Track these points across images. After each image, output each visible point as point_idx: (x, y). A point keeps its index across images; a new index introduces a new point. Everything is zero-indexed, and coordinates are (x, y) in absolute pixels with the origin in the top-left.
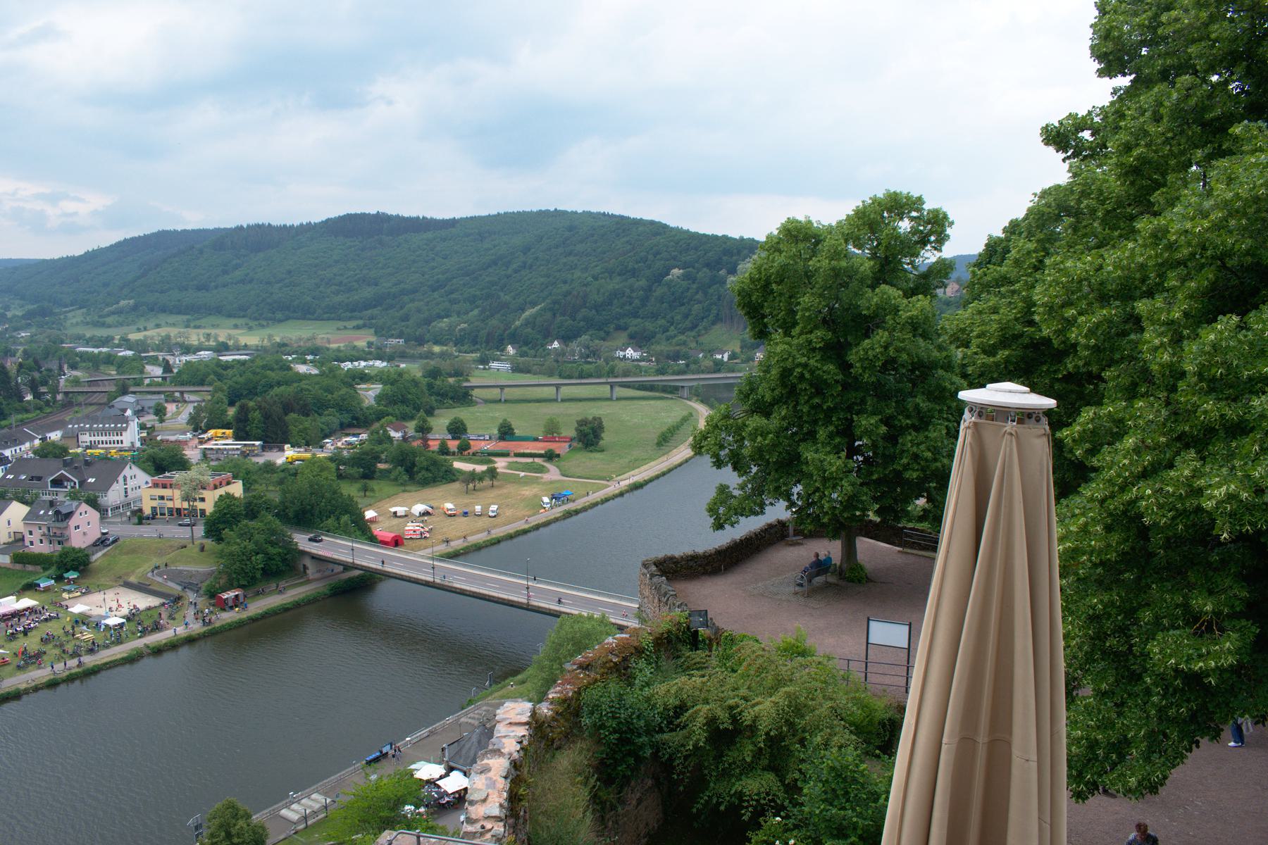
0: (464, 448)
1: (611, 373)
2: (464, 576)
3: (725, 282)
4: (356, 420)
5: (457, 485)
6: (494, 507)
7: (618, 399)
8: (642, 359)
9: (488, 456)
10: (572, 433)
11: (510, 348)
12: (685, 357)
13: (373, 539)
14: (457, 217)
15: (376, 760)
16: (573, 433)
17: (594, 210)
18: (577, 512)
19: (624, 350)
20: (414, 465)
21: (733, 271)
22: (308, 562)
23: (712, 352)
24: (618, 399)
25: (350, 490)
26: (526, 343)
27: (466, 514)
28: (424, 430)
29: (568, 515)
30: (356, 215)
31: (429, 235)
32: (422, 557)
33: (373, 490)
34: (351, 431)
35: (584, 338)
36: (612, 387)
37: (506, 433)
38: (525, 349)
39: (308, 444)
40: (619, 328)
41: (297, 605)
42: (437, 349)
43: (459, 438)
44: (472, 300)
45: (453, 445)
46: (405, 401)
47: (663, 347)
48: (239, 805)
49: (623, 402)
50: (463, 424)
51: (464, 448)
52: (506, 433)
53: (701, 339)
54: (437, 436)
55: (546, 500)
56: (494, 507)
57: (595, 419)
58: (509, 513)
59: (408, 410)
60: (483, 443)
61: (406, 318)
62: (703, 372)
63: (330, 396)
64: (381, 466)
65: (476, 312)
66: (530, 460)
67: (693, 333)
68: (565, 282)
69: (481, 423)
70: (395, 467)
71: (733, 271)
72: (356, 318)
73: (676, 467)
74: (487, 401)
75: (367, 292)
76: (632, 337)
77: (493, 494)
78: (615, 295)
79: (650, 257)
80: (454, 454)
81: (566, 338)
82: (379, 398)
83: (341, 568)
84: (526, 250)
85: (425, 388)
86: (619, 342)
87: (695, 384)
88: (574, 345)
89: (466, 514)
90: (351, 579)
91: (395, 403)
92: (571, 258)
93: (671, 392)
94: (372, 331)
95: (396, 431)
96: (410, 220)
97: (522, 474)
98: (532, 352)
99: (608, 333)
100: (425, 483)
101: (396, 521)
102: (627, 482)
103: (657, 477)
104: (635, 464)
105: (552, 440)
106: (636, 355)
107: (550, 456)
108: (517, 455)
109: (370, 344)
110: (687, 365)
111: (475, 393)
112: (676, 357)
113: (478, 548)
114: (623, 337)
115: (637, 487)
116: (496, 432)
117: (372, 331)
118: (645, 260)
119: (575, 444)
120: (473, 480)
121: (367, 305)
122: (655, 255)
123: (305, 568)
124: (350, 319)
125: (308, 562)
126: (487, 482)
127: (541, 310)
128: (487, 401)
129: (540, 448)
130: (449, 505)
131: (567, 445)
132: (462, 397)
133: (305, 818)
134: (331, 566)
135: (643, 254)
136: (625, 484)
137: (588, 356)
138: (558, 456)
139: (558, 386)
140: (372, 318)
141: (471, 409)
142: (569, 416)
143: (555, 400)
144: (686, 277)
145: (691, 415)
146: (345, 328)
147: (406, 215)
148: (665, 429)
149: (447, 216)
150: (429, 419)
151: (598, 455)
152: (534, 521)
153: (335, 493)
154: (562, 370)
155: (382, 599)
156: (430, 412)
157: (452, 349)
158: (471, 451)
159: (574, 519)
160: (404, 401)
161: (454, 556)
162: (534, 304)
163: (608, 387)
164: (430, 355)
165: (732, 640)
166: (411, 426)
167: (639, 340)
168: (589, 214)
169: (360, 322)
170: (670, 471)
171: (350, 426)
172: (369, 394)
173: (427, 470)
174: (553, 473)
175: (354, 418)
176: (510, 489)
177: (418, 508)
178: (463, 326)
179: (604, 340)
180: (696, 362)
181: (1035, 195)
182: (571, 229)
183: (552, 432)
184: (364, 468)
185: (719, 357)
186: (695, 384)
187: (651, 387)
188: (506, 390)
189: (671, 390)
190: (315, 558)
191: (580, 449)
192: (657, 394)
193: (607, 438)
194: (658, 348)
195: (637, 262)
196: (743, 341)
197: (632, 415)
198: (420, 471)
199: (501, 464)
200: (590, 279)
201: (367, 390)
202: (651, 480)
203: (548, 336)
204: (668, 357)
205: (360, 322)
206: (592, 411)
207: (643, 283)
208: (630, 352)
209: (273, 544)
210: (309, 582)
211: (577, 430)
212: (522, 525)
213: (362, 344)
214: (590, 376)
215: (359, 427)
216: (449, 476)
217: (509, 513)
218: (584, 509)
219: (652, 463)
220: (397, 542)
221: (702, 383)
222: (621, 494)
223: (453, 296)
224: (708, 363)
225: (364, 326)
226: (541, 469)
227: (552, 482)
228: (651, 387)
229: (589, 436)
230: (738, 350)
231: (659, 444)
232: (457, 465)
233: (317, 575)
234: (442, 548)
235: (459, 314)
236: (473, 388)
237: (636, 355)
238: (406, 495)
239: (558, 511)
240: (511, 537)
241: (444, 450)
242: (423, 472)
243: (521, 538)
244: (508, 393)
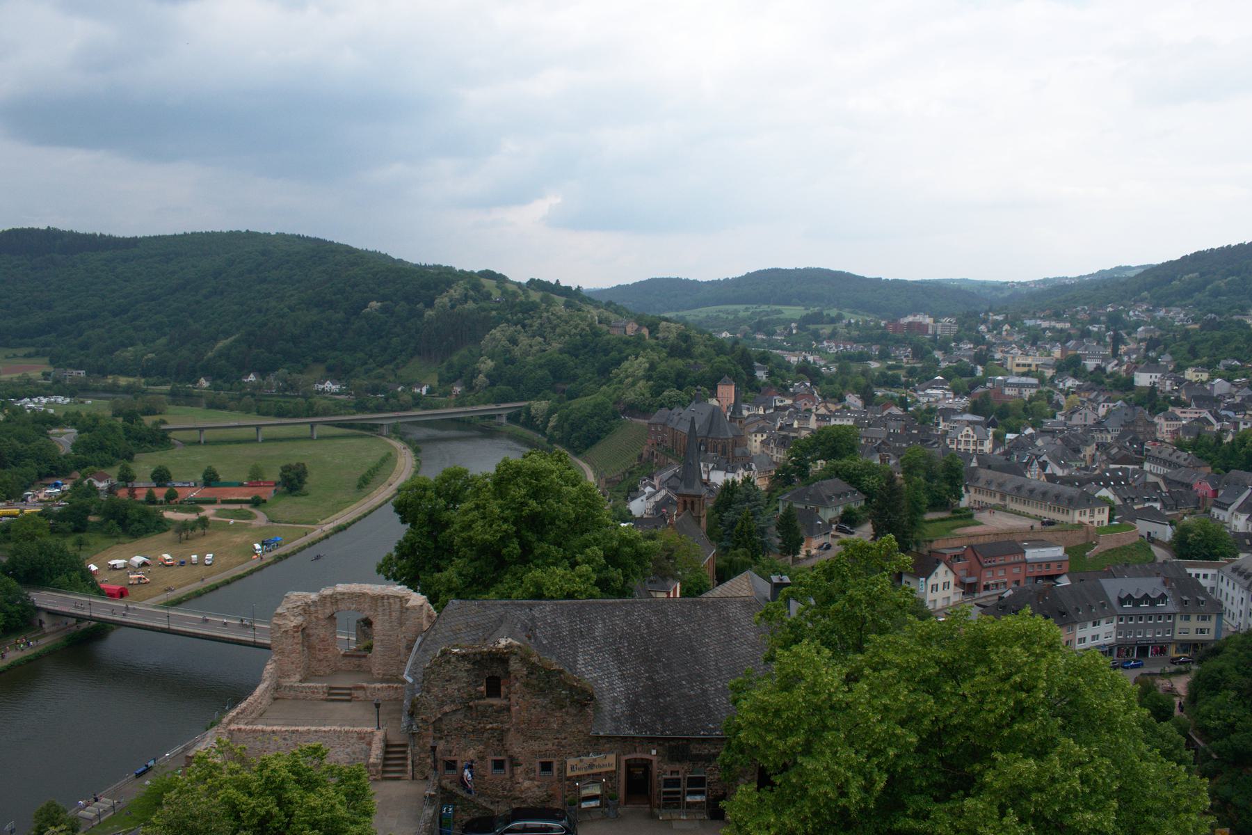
0: (171, 497)
1: (310, 411)
2: (188, 620)
3: (422, 315)
4: (53, 470)
5: (170, 535)
6: (209, 556)
7: (321, 438)
9: (194, 505)
10: (276, 477)
11: (202, 380)
12: (384, 391)
13: (101, 593)
15: (144, 772)
16: (277, 478)
17: (288, 232)
18: (286, 556)
20: (126, 516)
21: (430, 305)
22: (43, 617)
23: (410, 385)
24: (321, 438)
25: (69, 544)
26: (221, 377)
27: (182, 563)
28: (127, 478)
29: (280, 558)
30: (23, 230)
32: (147, 606)
33: (88, 544)
34: (51, 481)
35: (282, 371)
37: (210, 479)
38: (219, 382)
39: (8, 498)
40: (316, 360)
41: (39, 657)
42: (123, 381)
43: (164, 486)
45: (160, 493)
46: (100, 447)
47: (363, 382)
48: (58, 803)
49: (326, 442)
50: (168, 472)
51: (171, 497)
52: (210, 479)
53: (399, 372)
54: (141, 485)
55: (258, 546)
56: (209, 556)
57: (298, 464)
58: (223, 560)
59: (107, 457)
60: (189, 490)
61: (85, 346)
63: (26, 447)
64: (92, 519)
65: (163, 340)
66: (237, 507)
67: (391, 366)
68: (260, 311)
69: (186, 466)
70: (107, 521)
71: (430, 305)
72: (27, 346)
73: (376, 508)
74: (185, 443)
76: (330, 369)
77: (205, 542)
80: (161, 503)
81: (263, 372)
82: (75, 446)
83: (74, 620)
85: (121, 432)
87: (394, 421)
88: (271, 378)
89: (182, 563)
90: (85, 630)
91: (94, 451)
93: (370, 430)
94: (47, 359)
95: (100, 481)
96: (85, 237)
97: (232, 522)
98: (228, 385)
99: (306, 366)
100: (136, 535)
101: (116, 574)
102: (332, 525)
103: (359, 519)
104: (338, 507)
105: (257, 485)
106: (335, 388)
107: (257, 502)
108: (224, 502)
109: (46, 375)
110: (387, 399)
111: (171, 435)
112: (375, 390)
113: (199, 594)
114: (320, 370)
115: (340, 529)
116: (200, 477)
117: (47, 359)
119: (280, 488)
120: (186, 530)
123: (41, 622)
125: (43, 617)
126: (199, 531)
127: (235, 341)
128: (185, 443)
129: (245, 494)
130: (167, 556)
131: (272, 490)
132: (159, 439)
133: (99, 816)
134: (65, 619)
136: (328, 528)
137: (286, 390)
138: (265, 501)
140: (46, 345)
141: (170, 453)
142: (274, 461)
143: (256, 440)
144: (384, 310)
145: (390, 454)
146: (15, 356)
148: (365, 471)
149: (128, 234)
150: (131, 465)
151: (302, 499)
152: (248, 567)
153: (62, 551)
154: (258, 404)
155: (113, 646)
156: (129, 457)
157: (141, 382)
158: (178, 500)
159: (285, 562)
160: (102, 448)
161: (177, 603)
162: (227, 334)
163: (308, 426)
164: (114, 389)
165: (388, 578)
166: (114, 472)
167: (335, 373)
169: (32, 350)
170: (371, 512)
171: (49, 475)
172: (65, 439)
173: (139, 521)
174: (260, 519)
175: (52, 468)
176: (220, 536)
177: (138, 559)
178: (150, 356)
179: (301, 372)
180: (395, 396)
183: (256, 478)
184: (74, 520)
185: (417, 390)
186: (394, 421)
187: (350, 425)
189: (372, 429)
190: (50, 613)
191: (285, 494)
192: (357, 432)
193: (311, 480)
194: (358, 382)
196: (440, 375)
197: (331, 456)
198: (131, 523)
199: (209, 511)
200: (286, 310)
201: (61, 435)
202: (354, 522)
203: (244, 369)
204: (367, 391)
205: (32, 350)
206: (297, 454)
207: (340, 315)
208: (329, 386)
209: (12, 603)
210: (45, 635)
211: (281, 475)
212: (239, 571)
213: (36, 374)
215: (57, 476)
216: (161, 526)
217: (223, 560)
218: (293, 553)
219: (355, 506)
220: (122, 594)
222: (327, 537)
223: (138, 323)
224: (407, 397)
225: (37, 354)
226: (249, 516)
227: (261, 528)
228: (350, 425)
229: (293, 482)
230: (436, 383)
231: (360, 487)
232: (168, 515)
233: (54, 628)
234: (164, 597)
235: (144, 342)
237: (335, 388)
238: (121, 547)
239: (269, 557)
240: (227, 583)
241: (151, 500)
242: (136, 524)
243: (237, 583)
244: (207, 435)
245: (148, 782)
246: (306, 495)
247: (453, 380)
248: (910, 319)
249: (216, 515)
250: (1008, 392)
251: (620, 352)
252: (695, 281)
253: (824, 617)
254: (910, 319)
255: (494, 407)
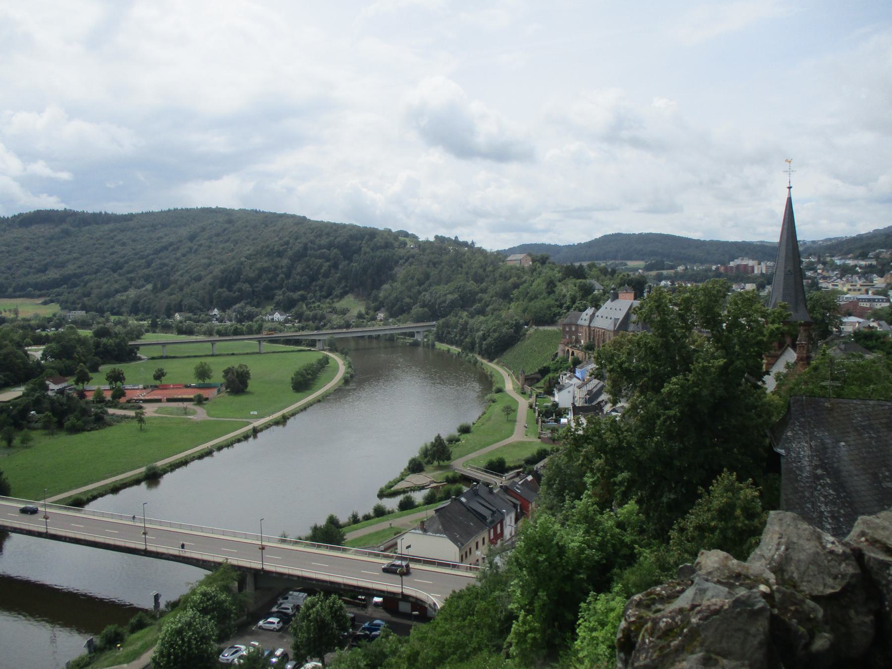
8: (286, 321)
14: (134, 212)
19: (273, 314)
31: (106, 227)
36: (260, 342)
44: (147, 279)
60: (138, 392)
75: (53, 274)
78: (264, 270)
84: (192, 238)
92: (228, 244)
118: (287, 243)
121: (56, 284)
122: (296, 239)
124: (40, 296)
138: (207, 399)
139: (213, 342)
169: (48, 299)
181: (454, 592)
188: (168, 347)
193: (252, 385)
195: (282, 245)
203: (210, 305)
205: (48, 299)
206: (234, 363)
208: (277, 316)
214: (242, 333)
225: (52, 301)
245: (689, 285)
246: (248, 393)
247: (377, 309)
248: (738, 262)
249: (156, 412)
250: (862, 304)
251: (519, 277)
252: (556, 246)
253: (822, 512)
254: (738, 262)
255: (415, 325)
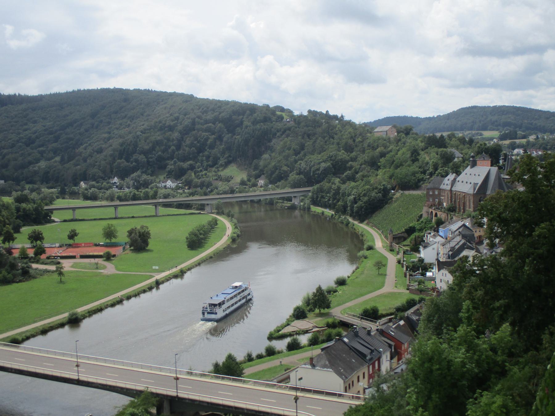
11: (82, 183)
19: (166, 182)
44: (56, 152)
62: (221, 194)
74: (460, 241)
78: (158, 143)
79: (181, 117)
84: (93, 115)
86: (162, 177)
108: (82, 257)
118: (177, 119)
122: (185, 115)
128: (460, 241)
135: (177, 115)
138: (114, 256)
139: (116, 207)
147: (169, 92)
168: (138, 91)
182: (125, 100)
188: (77, 211)
195: (173, 121)
206: (137, 224)
214: (139, 199)
221: (222, 201)
236: (51, 211)
243: (96, 317)
